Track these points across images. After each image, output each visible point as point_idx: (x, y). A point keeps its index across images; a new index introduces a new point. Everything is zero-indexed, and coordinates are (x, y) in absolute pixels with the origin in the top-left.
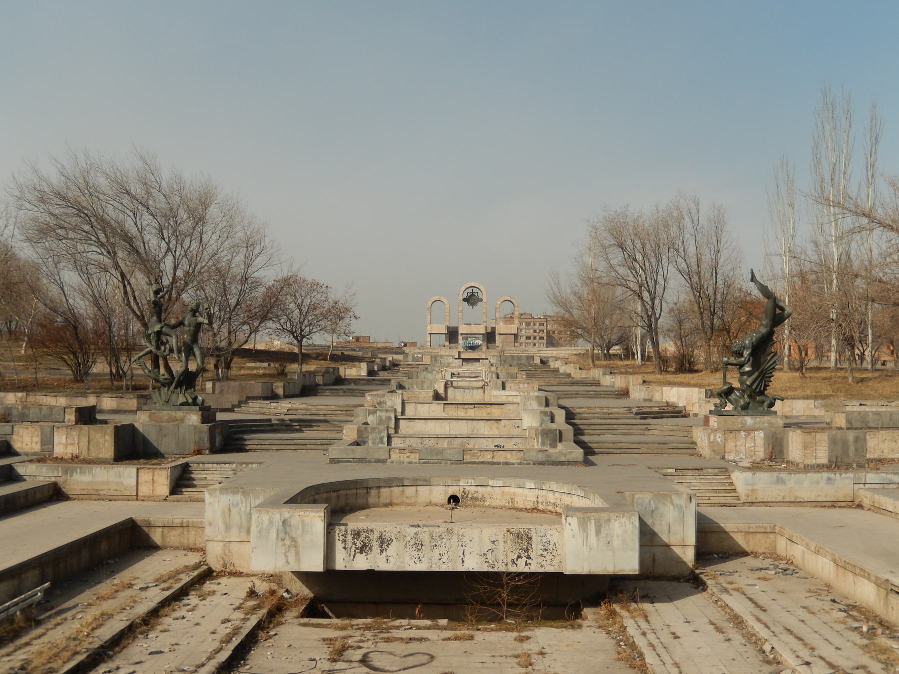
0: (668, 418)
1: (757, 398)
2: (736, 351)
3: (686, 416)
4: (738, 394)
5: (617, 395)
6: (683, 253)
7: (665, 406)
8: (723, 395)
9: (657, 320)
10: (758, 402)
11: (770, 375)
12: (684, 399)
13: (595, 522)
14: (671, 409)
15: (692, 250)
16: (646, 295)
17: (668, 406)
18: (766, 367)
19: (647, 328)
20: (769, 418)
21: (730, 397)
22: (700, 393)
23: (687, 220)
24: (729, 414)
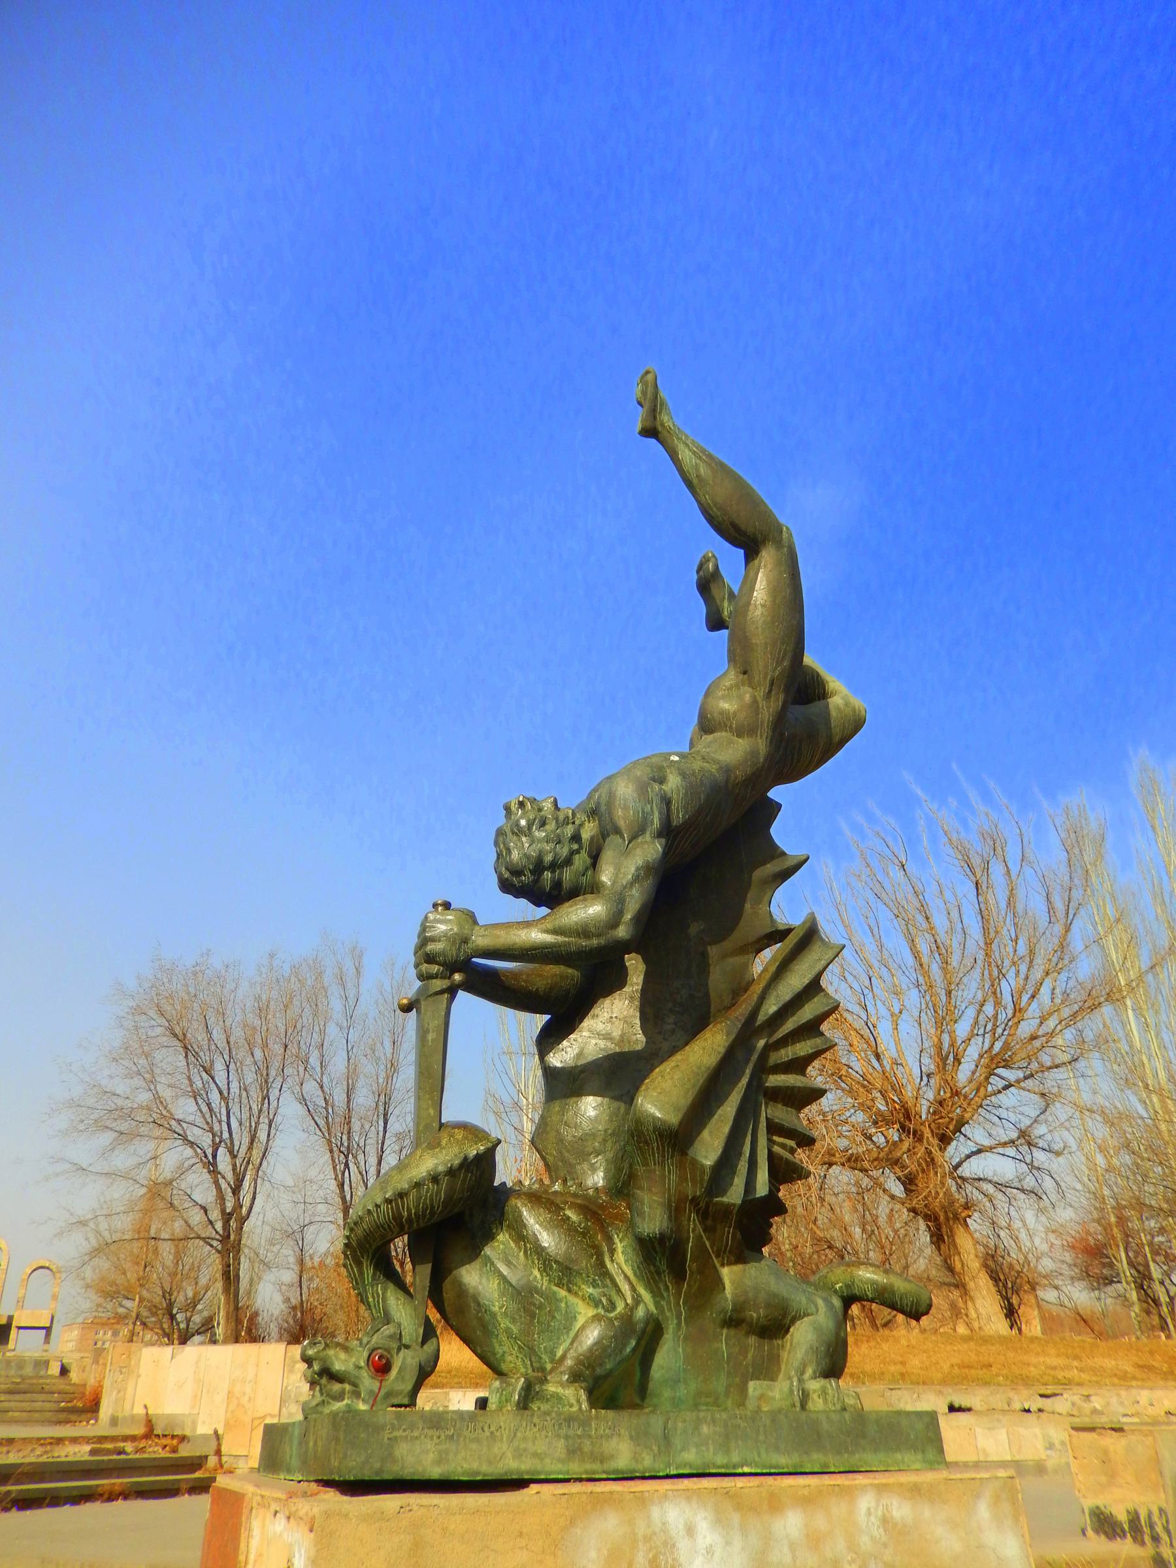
0: (111, 1497)
1: (727, 1273)
2: (539, 867)
3: (318, 1481)
4: (547, 1239)
5: (63, 1410)
6: (318, 1069)
7: (133, 1438)
8: (400, 1245)
9: (243, 1221)
10: (734, 1321)
14: (156, 1451)
15: (338, 1065)
16: (224, 1162)
17: (149, 1434)
18: (771, 1007)
20: (900, 1510)
21: (471, 1276)
23: (335, 991)
24: (462, 1465)
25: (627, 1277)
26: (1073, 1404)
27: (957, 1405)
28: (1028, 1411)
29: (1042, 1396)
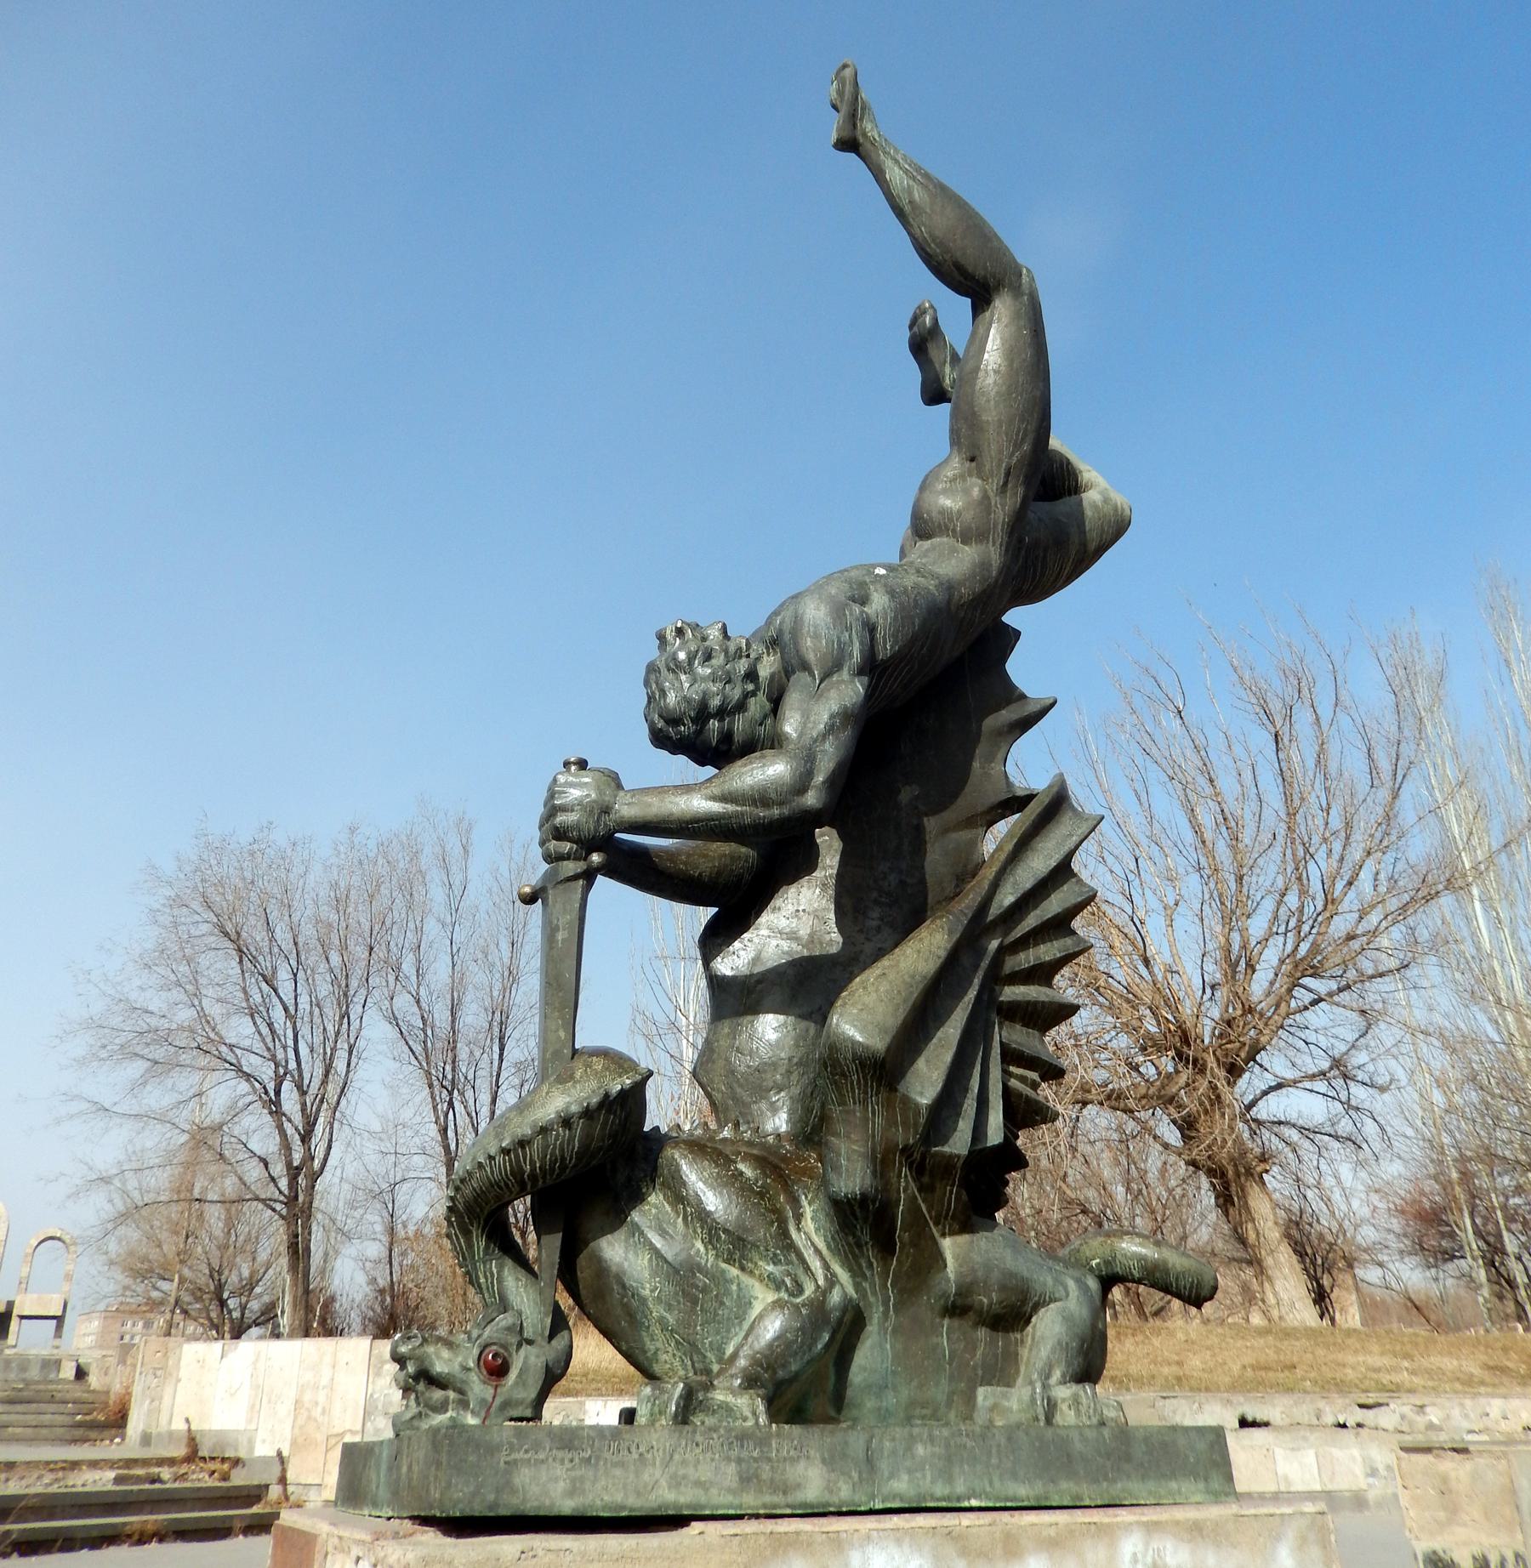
0: (142, 1539)
1: (950, 1246)
2: (702, 713)
5: (79, 1425)
6: (414, 978)
8: (520, 1208)
10: (958, 1308)
11: (1047, 951)
12: (285, 1409)
13: (1011, 929)
14: (200, 1479)
15: (439, 973)
16: (290, 1100)
17: (193, 1456)
19: (278, 1207)
21: (614, 1250)
22: (374, 1369)
23: (435, 877)
25: (817, 1251)
26: (1403, 1417)
27: (1250, 1419)
28: (1344, 1426)
29: (1361, 1406)
